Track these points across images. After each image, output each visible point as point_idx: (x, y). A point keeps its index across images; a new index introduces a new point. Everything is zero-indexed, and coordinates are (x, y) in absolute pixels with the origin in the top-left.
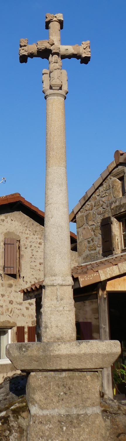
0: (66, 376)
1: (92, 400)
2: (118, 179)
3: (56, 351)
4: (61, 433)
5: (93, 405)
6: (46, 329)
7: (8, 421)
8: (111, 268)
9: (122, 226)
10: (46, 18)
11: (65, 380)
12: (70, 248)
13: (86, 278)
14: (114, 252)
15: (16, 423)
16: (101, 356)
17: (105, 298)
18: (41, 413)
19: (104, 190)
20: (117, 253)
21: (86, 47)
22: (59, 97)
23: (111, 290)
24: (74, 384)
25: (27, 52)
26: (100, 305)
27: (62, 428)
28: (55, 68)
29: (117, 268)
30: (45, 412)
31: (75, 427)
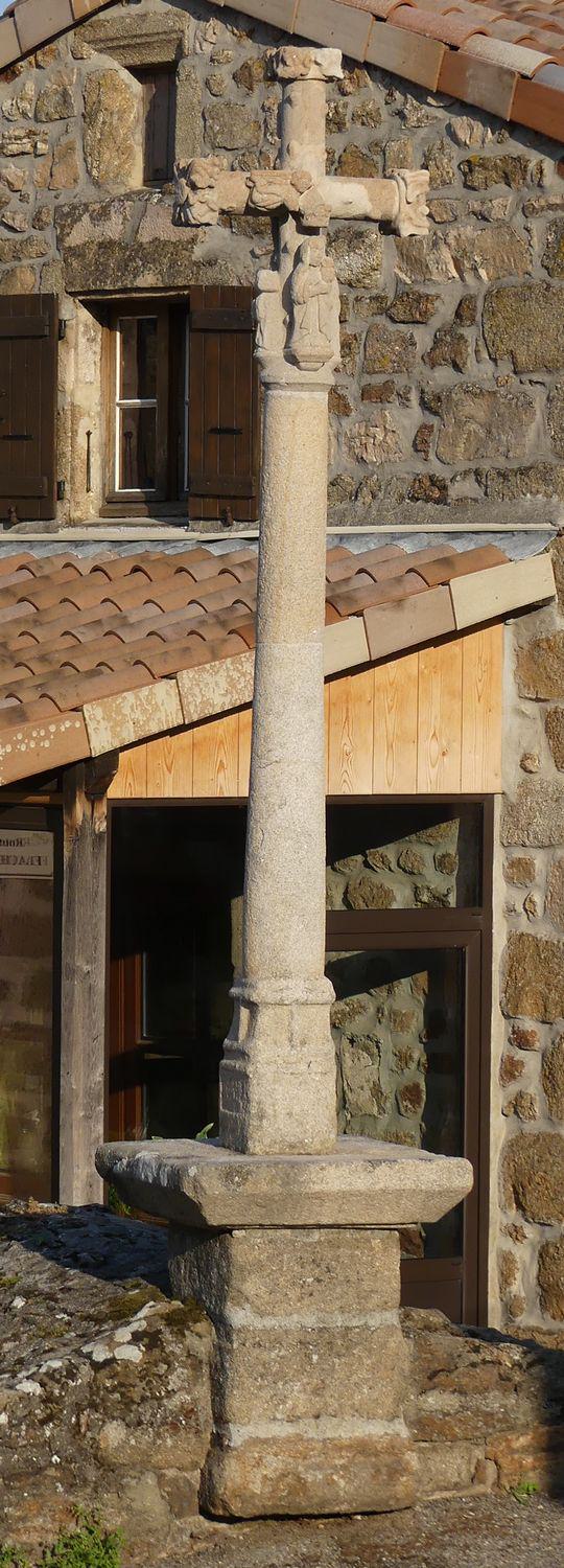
0: (322, 1239)
1: (382, 1297)
2: (127, 67)
3: (314, 1183)
4: (308, 1368)
5: (384, 1307)
6: (261, 1121)
7: (162, 1343)
8: (145, 691)
9: (122, 354)
11: (318, 1249)
13: (22, 741)
14: (61, 509)
15: (180, 1345)
16: (422, 1196)
17: (100, 836)
18: (258, 1323)
19: (24, 114)
20: (76, 515)
23: (129, 796)
24: (341, 1260)
26: (71, 867)
27: (308, 1357)
29: (174, 691)
30: (269, 1322)
31: (339, 1356)
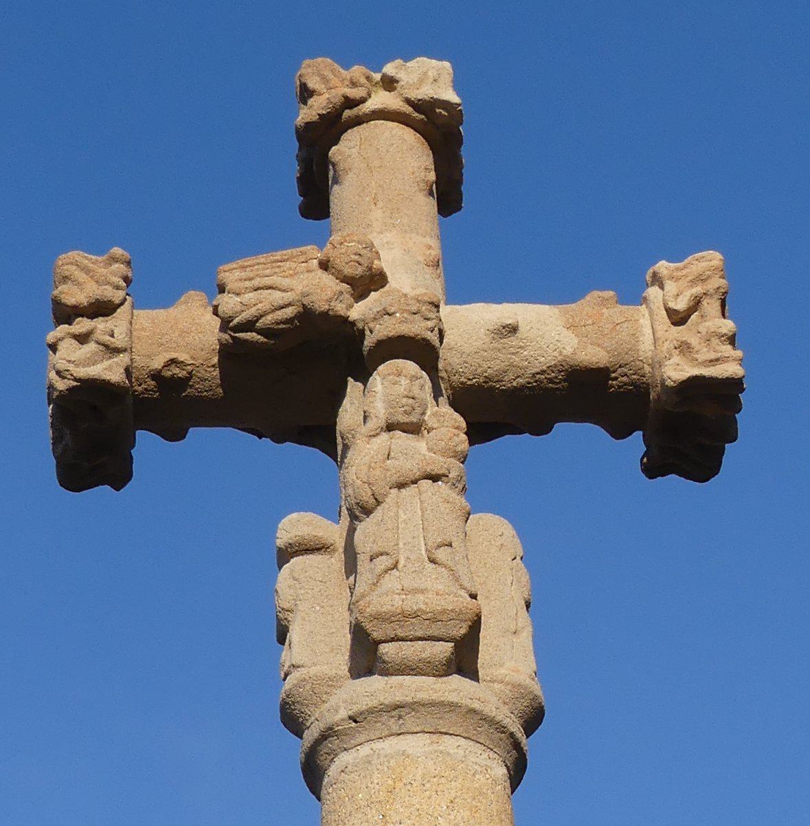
10: (306, 94)
12: (50, 464)
21: (696, 305)
22: (449, 743)
25: (123, 359)
28: (411, 467)
